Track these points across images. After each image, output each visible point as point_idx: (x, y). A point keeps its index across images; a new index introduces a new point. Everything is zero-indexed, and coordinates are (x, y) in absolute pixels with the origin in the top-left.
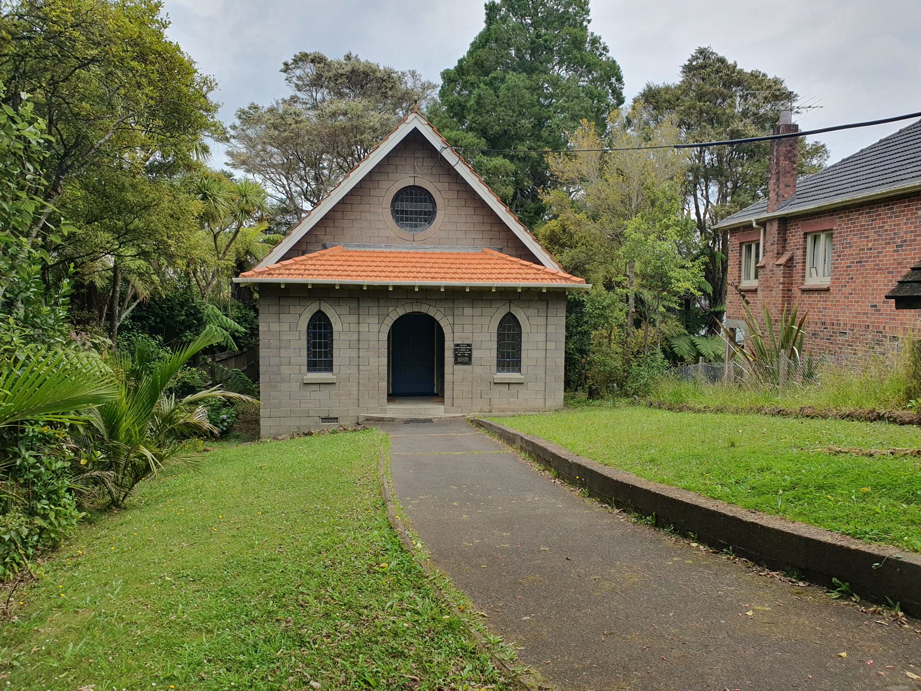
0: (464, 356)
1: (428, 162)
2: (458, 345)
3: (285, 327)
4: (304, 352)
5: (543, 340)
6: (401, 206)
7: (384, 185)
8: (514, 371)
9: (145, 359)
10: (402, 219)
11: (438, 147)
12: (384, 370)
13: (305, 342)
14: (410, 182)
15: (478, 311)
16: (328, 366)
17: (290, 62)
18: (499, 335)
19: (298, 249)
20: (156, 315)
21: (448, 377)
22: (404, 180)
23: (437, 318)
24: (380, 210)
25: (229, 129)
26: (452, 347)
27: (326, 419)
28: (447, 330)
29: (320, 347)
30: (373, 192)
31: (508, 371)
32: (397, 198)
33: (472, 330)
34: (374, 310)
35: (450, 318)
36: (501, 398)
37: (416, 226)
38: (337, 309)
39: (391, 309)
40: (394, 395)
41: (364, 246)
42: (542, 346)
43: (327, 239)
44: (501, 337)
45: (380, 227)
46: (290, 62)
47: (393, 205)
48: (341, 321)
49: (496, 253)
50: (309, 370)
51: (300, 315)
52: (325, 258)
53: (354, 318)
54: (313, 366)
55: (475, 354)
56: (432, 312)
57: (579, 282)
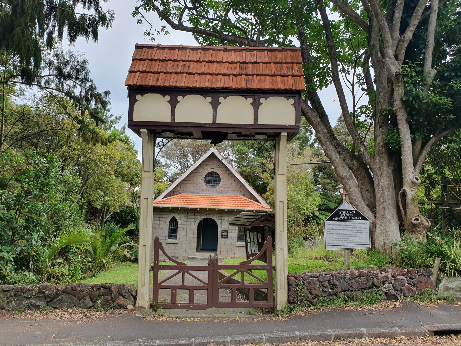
0: (225, 235)
1: (218, 163)
3: (161, 222)
6: (209, 179)
7: (202, 171)
9: (111, 232)
14: (211, 170)
16: (176, 237)
20: (119, 217)
22: (209, 169)
28: (219, 225)
30: (198, 174)
32: (207, 176)
34: (193, 217)
37: (213, 186)
38: (180, 216)
41: (194, 193)
43: (181, 190)
47: (205, 178)
48: (181, 220)
49: (241, 196)
50: (169, 238)
53: (185, 220)
54: (170, 237)
56: (214, 218)
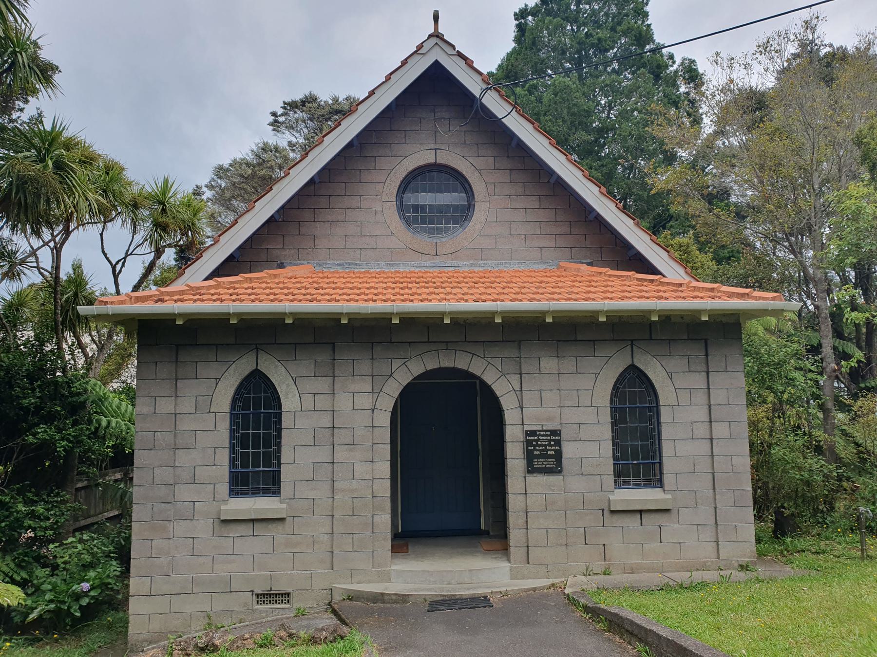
0: (546, 454)
2: (533, 433)
3: (187, 405)
4: (224, 456)
5: (706, 423)
6: (411, 198)
8: (648, 485)
10: (415, 221)
11: (476, 92)
12: (384, 488)
13: (226, 435)
15: (569, 364)
16: (271, 484)
17: (280, 111)
18: (614, 410)
19: (230, 266)
21: (514, 502)
22: (420, 155)
23: (489, 378)
24: (378, 205)
25: (204, 189)
26: (521, 437)
27: (267, 597)
28: (508, 403)
29: (256, 446)
31: (637, 485)
32: (406, 185)
33: (558, 403)
34: (364, 367)
35: (515, 380)
36: (628, 545)
39: (396, 364)
40: (408, 536)
42: (702, 431)
44: (618, 415)
45: (378, 233)
46: (280, 111)
48: (299, 393)
49: (584, 267)
51: (217, 380)
52: (277, 280)
53: (322, 384)
54: (241, 483)
55: (569, 450)
57: (773, 299)
